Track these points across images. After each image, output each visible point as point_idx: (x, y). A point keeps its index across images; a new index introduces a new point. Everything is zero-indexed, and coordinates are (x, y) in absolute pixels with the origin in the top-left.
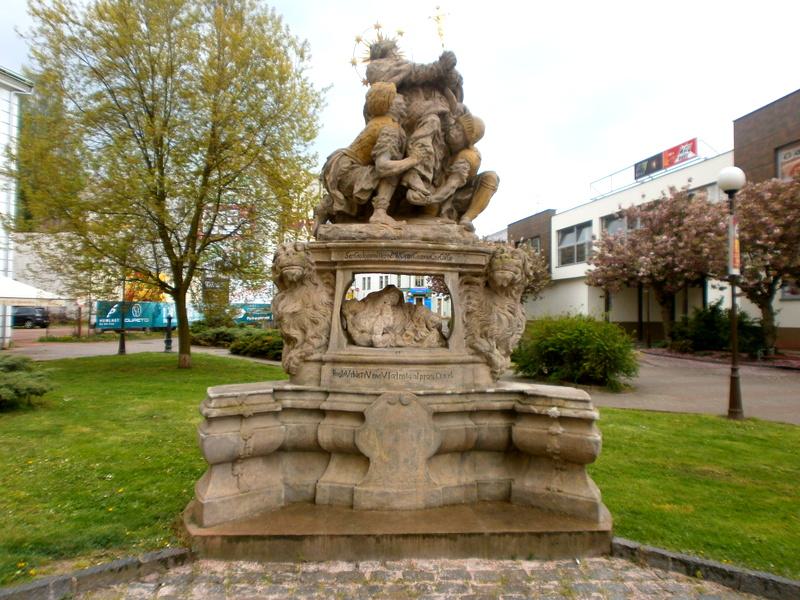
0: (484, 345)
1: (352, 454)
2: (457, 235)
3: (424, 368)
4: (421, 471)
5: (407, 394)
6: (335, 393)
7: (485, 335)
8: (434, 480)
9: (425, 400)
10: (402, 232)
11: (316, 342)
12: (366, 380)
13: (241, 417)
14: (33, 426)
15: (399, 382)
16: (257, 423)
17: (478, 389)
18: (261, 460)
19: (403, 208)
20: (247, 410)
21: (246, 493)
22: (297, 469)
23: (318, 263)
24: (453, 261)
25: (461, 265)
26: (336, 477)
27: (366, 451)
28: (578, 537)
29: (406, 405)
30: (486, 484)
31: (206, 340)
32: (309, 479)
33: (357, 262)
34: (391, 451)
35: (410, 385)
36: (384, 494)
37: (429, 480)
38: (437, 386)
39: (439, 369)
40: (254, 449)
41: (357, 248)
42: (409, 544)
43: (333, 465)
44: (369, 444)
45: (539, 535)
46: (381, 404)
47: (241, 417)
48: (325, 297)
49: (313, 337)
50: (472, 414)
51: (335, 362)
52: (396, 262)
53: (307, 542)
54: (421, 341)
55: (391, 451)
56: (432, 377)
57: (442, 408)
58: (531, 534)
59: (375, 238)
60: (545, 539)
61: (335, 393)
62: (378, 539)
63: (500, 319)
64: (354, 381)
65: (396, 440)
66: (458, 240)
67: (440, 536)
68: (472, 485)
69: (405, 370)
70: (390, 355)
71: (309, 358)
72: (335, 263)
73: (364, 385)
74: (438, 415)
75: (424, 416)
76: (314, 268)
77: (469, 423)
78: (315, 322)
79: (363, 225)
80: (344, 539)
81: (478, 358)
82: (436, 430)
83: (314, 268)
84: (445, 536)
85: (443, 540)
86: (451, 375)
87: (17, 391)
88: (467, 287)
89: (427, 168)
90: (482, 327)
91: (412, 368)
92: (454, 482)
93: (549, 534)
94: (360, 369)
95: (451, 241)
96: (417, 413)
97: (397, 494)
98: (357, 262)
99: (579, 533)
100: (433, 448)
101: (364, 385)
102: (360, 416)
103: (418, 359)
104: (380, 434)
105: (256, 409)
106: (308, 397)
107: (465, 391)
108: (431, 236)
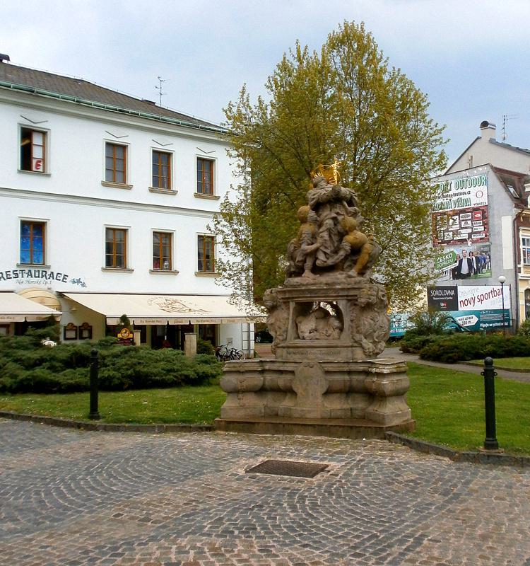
0: (358, 337)
1: (289, 391)
2: (344, 280)
3: (326, 349)
4: (320, 400)
5: (312, 363)
6: (287, 362)
7: (358, 332)
8: (326, 405)
9: (323, 365)
10: (317, 281)
11: (281, 338)
12: (298, 356)
13: (238, 372)
14: (200, 391)
15: (311, 356)
16: (247, 376)
17: (355, 361)
18: (253, 394)
19: (316, 270)
20: (241, 369)
21: (243, 407)
22: (274, 400)
23: (282, 298)
24: (340, 294)
25: (347, 296)
26: (286, 403)
27: (295, 389)
28: (369, 429)
29: (311, 367)
30: (356, 409)
31: (414, 348)
32: (277, 404)
33: (296, 298)
34: (305, 390)
35: (317, 358)
36: (303, 410)
37: (324, 405)
38: (331, 359)
39: (332, 349)
40: (247, 387)
41: (297, 291)
42: (295, 428)
43: (287, 397)
44: (298, 388)
45: (351, 427)
46: (301, 366)
47: (238, 372)
48: (285, 315)
49: (279, 335)
50: (349, 373)
51: (288, 347)
52: (310, 297)
53: (256, 425)
54: (329, 336)
55: (305, 390)
56: (328, 354)
57: (330, 369)
58: (348, 426)
59: (303, 285)
60: (354, 430)
61: (287, 362)
62: (284, 425)
63: (364, 324)
64: (294, 356)
65: (307, 385)
66: (344, 283)
67: (309, 425)
68: (348, 409)
69: (315, 350)
70: (308, 343)
71: (279, 346)
72: (289, 298)
73: (297, 358)
74: (327, 372)
75: (320, 373)
76: (281, 301)
77: (347, 377)
78: (280, 328)
79: (299, 278)
80: (270, 425)
81: (356, 344)
82: (326, 380)
83: (281, 301)
84: (311, 425)
85: (310, 427)
86: (339, 353)
87: (198, 374)
88: (354, 307)
89: (326, 248)
90: (357, 327)
91: (319, 349)
92: (339, 407)
93: (356, 427)
94: (296, 350)
95: (339, 284)
96: (317, 372)
97: (308, 411)
98: (296, 298)
99: (370, 427)
100: (324, 390)
101: (297, 358)
102: (292, 372)
103: (305, 345)
104: (300, 381)
105: (246, 369)
106: (278, 364)
107: (346, 360)
108: (329, 282)
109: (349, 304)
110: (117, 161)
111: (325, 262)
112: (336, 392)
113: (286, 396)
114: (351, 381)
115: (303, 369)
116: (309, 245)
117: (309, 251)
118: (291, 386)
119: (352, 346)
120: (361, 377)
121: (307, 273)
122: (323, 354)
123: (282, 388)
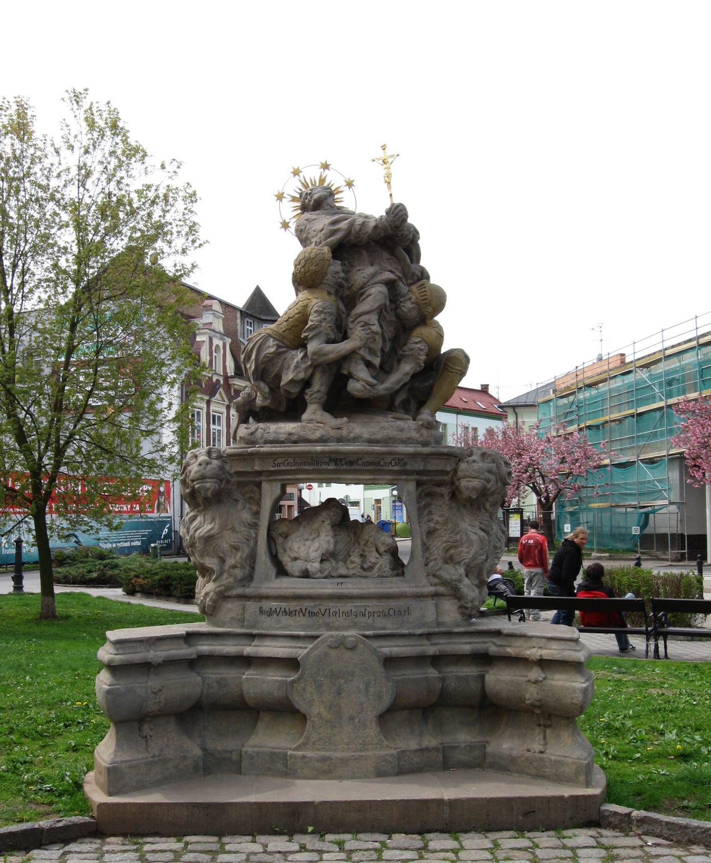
2: (414, 434)
9: (375, 644)
27: (301, 706)
43: (261, 725)
48: (246, 516)
50: (436, 660)
54: (371, 568)
56: (385, 615)
71: (229, 593)
72: (260, 473)
74: (390, 662)
77: (432, 672)
97: (342, 759)
100: (387, 701)
109: (675, 580)
110: (624, 525)
111: (372, 386)
112: (404, 708)
113: (256, 720)
114: (443, 679)
115: (326, 655)
116: (328, 342)
117: (331, 356)
118: (287, 698)
119: (436, 595)
120: (469, 671)
121: (312, 412)
122: (372, 614)
123: (251, 705)
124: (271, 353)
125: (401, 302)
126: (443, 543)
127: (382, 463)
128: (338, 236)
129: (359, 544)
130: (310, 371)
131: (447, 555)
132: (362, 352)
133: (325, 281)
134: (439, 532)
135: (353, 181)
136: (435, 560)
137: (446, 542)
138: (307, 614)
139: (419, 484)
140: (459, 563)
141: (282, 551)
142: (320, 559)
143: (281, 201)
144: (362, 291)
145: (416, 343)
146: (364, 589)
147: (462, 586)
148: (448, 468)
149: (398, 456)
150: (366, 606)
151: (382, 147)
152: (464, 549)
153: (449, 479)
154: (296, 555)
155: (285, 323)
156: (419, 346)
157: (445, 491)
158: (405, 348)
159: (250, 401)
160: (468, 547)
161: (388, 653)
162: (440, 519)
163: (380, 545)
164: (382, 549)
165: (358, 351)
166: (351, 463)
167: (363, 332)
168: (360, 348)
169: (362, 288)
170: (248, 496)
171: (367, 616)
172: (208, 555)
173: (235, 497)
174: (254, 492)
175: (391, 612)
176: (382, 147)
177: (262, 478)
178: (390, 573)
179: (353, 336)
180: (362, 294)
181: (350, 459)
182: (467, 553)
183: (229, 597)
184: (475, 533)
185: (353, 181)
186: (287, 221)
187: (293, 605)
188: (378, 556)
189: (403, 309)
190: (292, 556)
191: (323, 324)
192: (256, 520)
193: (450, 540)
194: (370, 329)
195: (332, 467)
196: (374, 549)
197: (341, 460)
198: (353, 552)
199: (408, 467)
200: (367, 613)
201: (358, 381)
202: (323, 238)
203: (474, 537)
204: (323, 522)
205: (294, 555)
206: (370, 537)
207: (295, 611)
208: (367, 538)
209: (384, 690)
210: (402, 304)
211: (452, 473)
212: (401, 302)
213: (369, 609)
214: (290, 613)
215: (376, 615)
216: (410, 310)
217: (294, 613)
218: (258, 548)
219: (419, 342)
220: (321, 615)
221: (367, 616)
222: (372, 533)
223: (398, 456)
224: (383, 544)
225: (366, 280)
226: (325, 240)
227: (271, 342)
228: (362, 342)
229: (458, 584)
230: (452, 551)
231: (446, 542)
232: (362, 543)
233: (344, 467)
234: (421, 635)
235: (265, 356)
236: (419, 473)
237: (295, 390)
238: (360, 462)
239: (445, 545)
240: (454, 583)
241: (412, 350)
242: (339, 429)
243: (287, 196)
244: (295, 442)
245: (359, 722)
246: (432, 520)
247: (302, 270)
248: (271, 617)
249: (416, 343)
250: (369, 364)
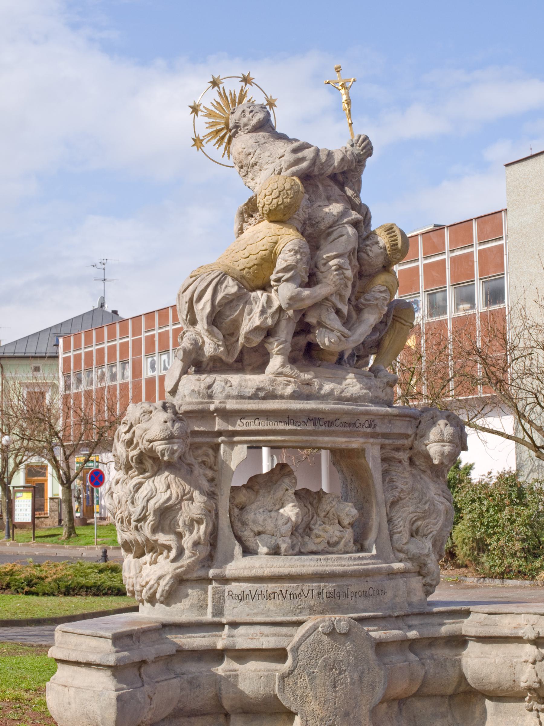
72: (220, 433)
124: (232, 294)
125: (367, 246)
126: (409, 513)
127: (357, 425)
128: (304, 165)
129: (318, 515)
130: (277, 317)
131: (414, 528)
132: (335, 299)
133: (296, 216)
134: (404, 501)
135: (275, 100)
136: (400, 532)
137: (413, 513)
138: (288, 596)
139: (383, 447)
140: (425, 536)
141: (240, 525)
142: (290, 533)
143: (197, 113)
144: (330, 230)
145: (381, 292)
146: (344, 566)
147: (429, 562)
148: (410, 432)
149: (371, 417)
150: (348, 585)
151: (336, 69)
152: (432, 520)
153: (410, 443)
154: (260, 529)
155: (243, 260)
156: (384, 295)
157: (404, 456)
158: (368, 296)
159: (198, 347)
160: (436, 518)
161: (378, 637)
162: (404, 487)
163: (343, 516)
164: (346, 522)
165: (330, 298)
166: (330, 423)
167: (337, 277)
168: (332, 295)
169: (331, 227)
170: (200, 460)
171: (350, 596)
172: (163, 531)
173: (188, 461)
174: (207, 455)
175: (371, 592)
176: (336, 69)
177: (220, 440)
178: (354, 548)
179: (324, 280)
180: (329, 234)
181: (328, 419)
182: (435, 524)
183: (187, 580)
184: (442, 503)
185: (275, 100)
186: (201, 138)
187: (271, 587)
188: (342, 529)
189: (370, 253)
190: (256, 530)
191: (299, 265)
192: (213, 489)
193: (418, 510)
194: (343, 273)
195: (310, 427)
196: (337, 521)
197: (319, 419)
198: (314, 525)
199: (378, 430)
200: (349, 593)
201: (333, 331)
202: (284, 165)
203: (442, 507)
204: (287, 490)
205: (257, 529)
206: (332, 507)
207: (274, 593)
208: (328, 508)
209: (377, 680)
210: (368, 248)
211: (412, 437)
212: (367, 246)
213: (352, 589)
214: (269, 597)
215: (358, 596)
216: (377, 256)
217: (272, 596)
218: (220, 522)
219: (384, 291)
220: (303, 597)
221: (350, 596)
222: (334, 503)
223: (371, 417)
224: (347, 515)
225: (336, 218)
226: (287, 169)
227: (229, 281)
228: (335, 288)
229: (426, 559)
230: (419, 523)
231: (413, 513)
232: (322, 514)
233: (323, 428)
234: (397, 617)
235: (224, 298)
236: (385, 436)
237: (257, 340)
238: (338, 422)
239: (411, 515)
240: (423, 558)
241: (377, 299)
242: (308, 384)
243: (204, 110)
244: (264, 398)
245: (354, 718)
246: (397, 487)
247: (275, 201)
248: (243, 602)
249: (381, 292)
250: (338, 312)
